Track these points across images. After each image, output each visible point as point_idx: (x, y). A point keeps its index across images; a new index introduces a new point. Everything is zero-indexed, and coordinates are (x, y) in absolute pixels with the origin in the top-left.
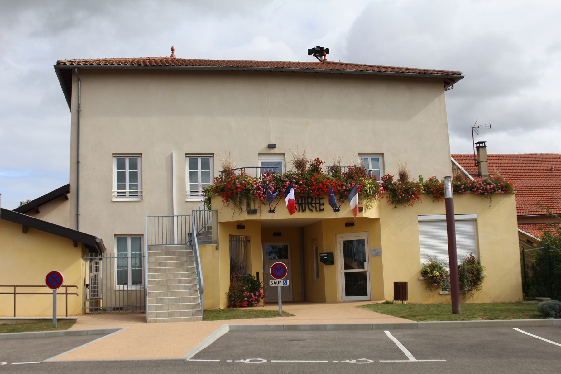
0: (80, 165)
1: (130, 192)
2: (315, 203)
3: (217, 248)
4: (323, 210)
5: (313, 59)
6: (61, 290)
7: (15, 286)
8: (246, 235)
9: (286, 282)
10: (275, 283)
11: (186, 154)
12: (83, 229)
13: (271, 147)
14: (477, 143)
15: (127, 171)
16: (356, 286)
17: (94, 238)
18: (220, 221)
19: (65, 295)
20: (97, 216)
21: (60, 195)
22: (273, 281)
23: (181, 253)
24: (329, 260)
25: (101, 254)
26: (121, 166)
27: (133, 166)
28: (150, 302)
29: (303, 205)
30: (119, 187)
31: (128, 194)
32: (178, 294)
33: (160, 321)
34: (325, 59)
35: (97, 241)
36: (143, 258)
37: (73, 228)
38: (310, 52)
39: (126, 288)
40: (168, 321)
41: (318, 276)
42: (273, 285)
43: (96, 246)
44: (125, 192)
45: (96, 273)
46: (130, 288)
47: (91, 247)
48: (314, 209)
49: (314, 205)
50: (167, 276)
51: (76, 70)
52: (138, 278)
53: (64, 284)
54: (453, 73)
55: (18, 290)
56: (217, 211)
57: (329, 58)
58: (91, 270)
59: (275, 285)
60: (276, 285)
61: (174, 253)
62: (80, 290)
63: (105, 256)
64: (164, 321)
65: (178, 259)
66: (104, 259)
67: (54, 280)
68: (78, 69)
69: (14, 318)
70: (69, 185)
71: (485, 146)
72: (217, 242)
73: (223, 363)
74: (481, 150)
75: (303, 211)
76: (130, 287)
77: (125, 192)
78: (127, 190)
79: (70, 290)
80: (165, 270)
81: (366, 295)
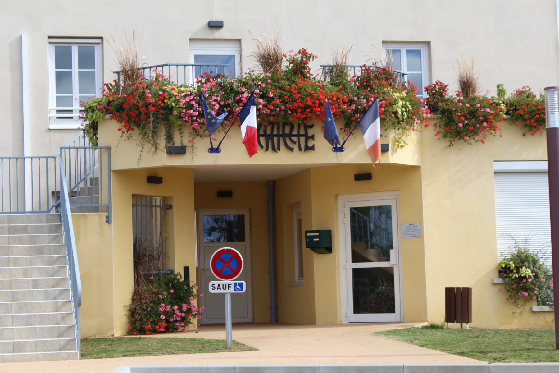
2: (298, 136)
3: (108, 221)
4: (313, 148)
9: (241, 285)
10: (219, 288)
11: (49, 37)
13: (215, 25)
16: (374, 294)
18: (115, 167)
22: (216, 283)
23: (38, 230)
24: (323, 243)
29: (275, 139)
32: (33, 307)
40: (13, 360)
41: (301, 275)
42: (216, 291)
48: (296, 147)
49: (295, 139)
56: (109, 149)
59: (219, 291)
60: (222, 291)
61: (25, 229)
65: (32, 240)
72: (108, 209)
75: (274, 150)
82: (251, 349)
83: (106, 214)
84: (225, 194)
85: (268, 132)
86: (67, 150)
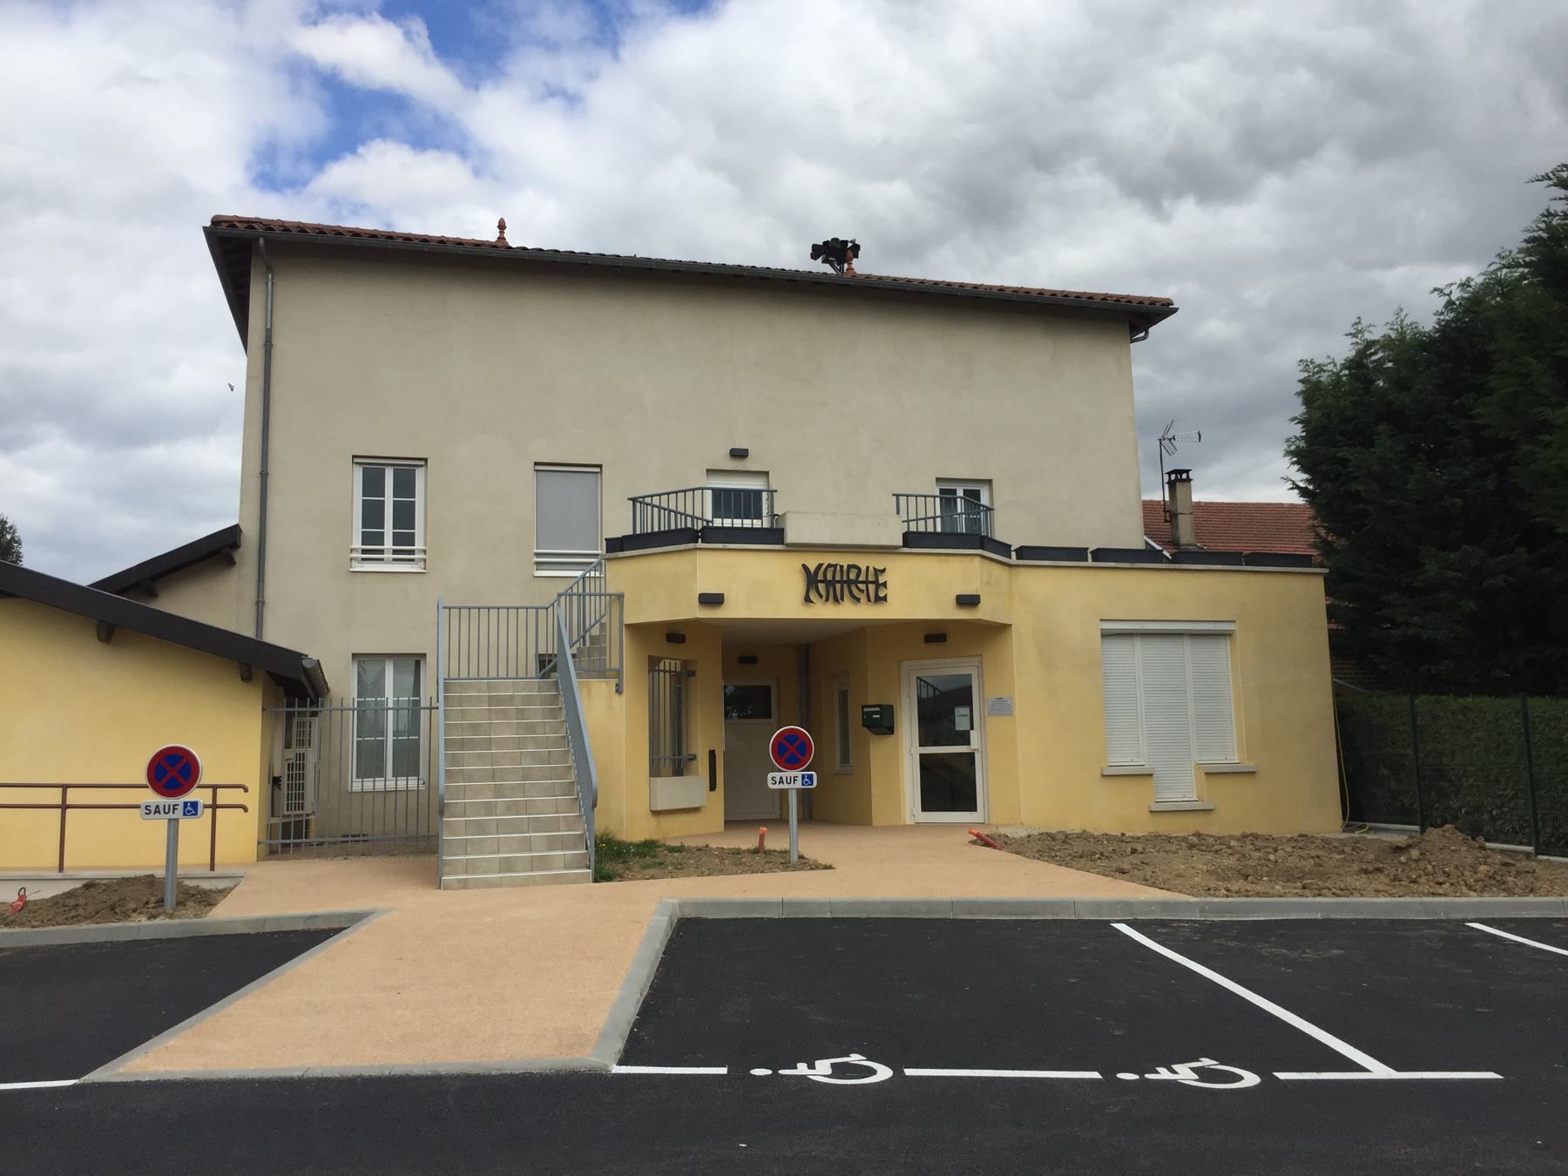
0: (272, 480)
1: (395, 552)
2: (866, 582)
3: (619, 691)
5: (820, 267)
6: (197, 795)
7: (65, 787)
8: (686, 657)
9: (810, 777)
10: (781, 782)
11: (536, 464)
12: (276, 635)
13: (739, 454)
14: (1170, 474)
15: (389, 499)
16: (949, 786)
17: (297, 657)
18: (627, 621)
19: (209, 811)
20: (314, 603)
21: (216, 553)
22: (777, 775)
23: (529, 700)
24: (882, 723)
25: (314, 703)
26: (373, 484)
27: (405, 485)
28: (453, 831)
29: (838, 586)
30: (366, 538)
31: (388, 556)
32: (526, 807)
33: (477, 884)
34: (850, 269)
35: (307, 664)
36: (424, 715)
37: (249, 632)
38: (817, 252)
39: (380, 784)
40: (498, 884)
41: (845, 759)
42: (777, 786)
43: (303, 679)
44: (382, 552)
45: (301, 751)
46: (391, 785)
47: (289, 685)
48: (863, 597)
49: (862, 586)
50: (493, 760)
51: (261, 241)
52: (408, 761)
53: (205, 778)
54: (1153, 302)
55: (74, 796)
56: (620, 597)
57: (862, 266)
58: (288, 745)
59: (781, 786)
60: (785, 786)
61: (511, 699)
62: (254, 798)
63: (327, 706)
64: (488, 884)
65: (520, 713)
66: (324, 714)
67: (173, 772)
68: (266, 240)
69: (60, 875)
70: (236, 527)
71: (1188, 480)
72: (618, 674)
73: (739, 1075)
74: (1179, 487)
75: (836, 600)
76: (389, 782)
77: (382, 552)
78: (388, 543)
79: (224, 796)
80: (489, 743)
81: (972, 807)
82: (816, 866)
83: (616, 681)
84: (748, 660)
85: (829, 577)
86: (532, 612)
